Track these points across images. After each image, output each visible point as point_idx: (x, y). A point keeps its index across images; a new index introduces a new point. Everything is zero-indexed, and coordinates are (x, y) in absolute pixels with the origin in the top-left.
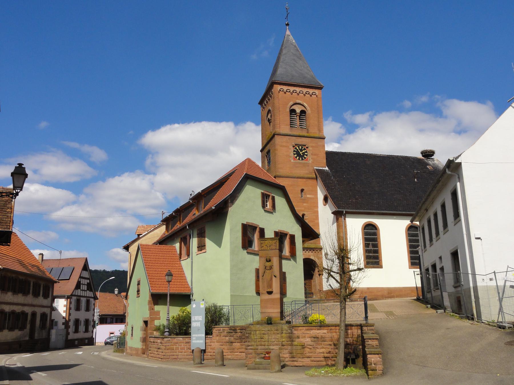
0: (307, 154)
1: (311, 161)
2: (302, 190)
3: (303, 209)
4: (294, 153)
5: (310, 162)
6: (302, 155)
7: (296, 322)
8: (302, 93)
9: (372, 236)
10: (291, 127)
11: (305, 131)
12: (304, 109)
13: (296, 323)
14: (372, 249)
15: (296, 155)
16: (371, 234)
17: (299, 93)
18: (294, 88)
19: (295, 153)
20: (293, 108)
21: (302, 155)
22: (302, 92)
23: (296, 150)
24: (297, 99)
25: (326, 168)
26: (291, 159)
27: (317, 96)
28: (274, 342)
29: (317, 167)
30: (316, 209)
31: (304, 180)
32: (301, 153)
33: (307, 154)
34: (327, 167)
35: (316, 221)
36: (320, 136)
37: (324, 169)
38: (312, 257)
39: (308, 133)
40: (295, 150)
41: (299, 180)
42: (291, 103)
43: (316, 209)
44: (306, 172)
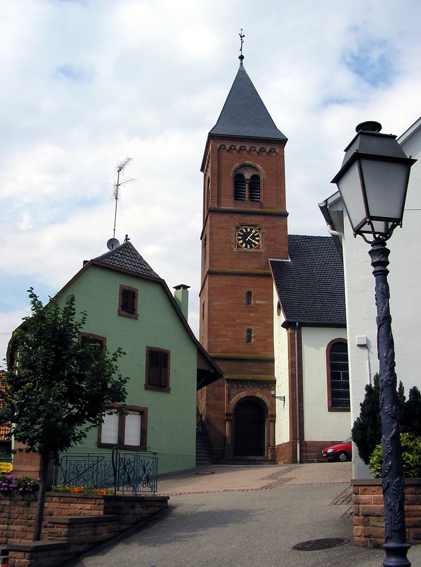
0: (258, 239)
1: (265, 250)
2: (249, 294)
3: (249, 321)
4: (238, 238)
5: (263, 251)
6: (247, 240)
7: (123, 491)
8: (255, 150)
9: (344, 361)
10: (251, 201)
11: (258, 204)
12: (256, 173)
13: (123, 493)
14: (343, 382)
15: (242, 241)
16: (342, 359)
17: (259, 151)
18: (242, 143)
19: (241, 238)
20: (240, 171)
21: (247, 240)
22: (254, 149)
23: (242, 234)
24: (246, 159)
25: (288, 260)
26: (233, 246)
27: (277, 154)
28: (17, 518)
29: (272, 258)
30: (269, 322)
31: (253, 278)
32: (249, 238)
33: (258, 239)
34: (289, 258)
35: (269, 340)
36: (279, 211)
37: (284, 260)
38: (259, 395)
39: (261, 207)
40: (240, 233)
41: (244, 278)
42: (237, 165)
43: (269, 322)
44: (255, 266)
